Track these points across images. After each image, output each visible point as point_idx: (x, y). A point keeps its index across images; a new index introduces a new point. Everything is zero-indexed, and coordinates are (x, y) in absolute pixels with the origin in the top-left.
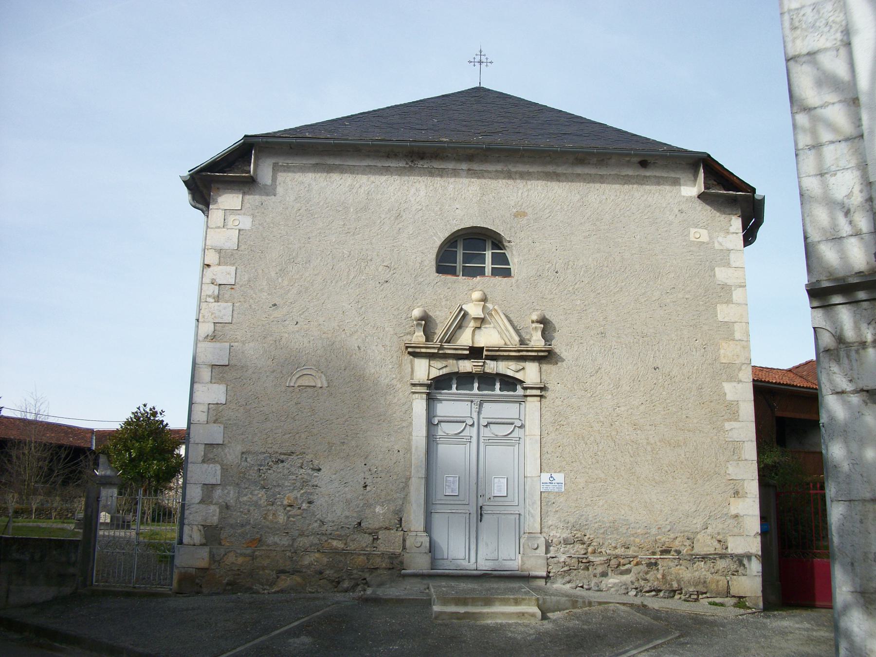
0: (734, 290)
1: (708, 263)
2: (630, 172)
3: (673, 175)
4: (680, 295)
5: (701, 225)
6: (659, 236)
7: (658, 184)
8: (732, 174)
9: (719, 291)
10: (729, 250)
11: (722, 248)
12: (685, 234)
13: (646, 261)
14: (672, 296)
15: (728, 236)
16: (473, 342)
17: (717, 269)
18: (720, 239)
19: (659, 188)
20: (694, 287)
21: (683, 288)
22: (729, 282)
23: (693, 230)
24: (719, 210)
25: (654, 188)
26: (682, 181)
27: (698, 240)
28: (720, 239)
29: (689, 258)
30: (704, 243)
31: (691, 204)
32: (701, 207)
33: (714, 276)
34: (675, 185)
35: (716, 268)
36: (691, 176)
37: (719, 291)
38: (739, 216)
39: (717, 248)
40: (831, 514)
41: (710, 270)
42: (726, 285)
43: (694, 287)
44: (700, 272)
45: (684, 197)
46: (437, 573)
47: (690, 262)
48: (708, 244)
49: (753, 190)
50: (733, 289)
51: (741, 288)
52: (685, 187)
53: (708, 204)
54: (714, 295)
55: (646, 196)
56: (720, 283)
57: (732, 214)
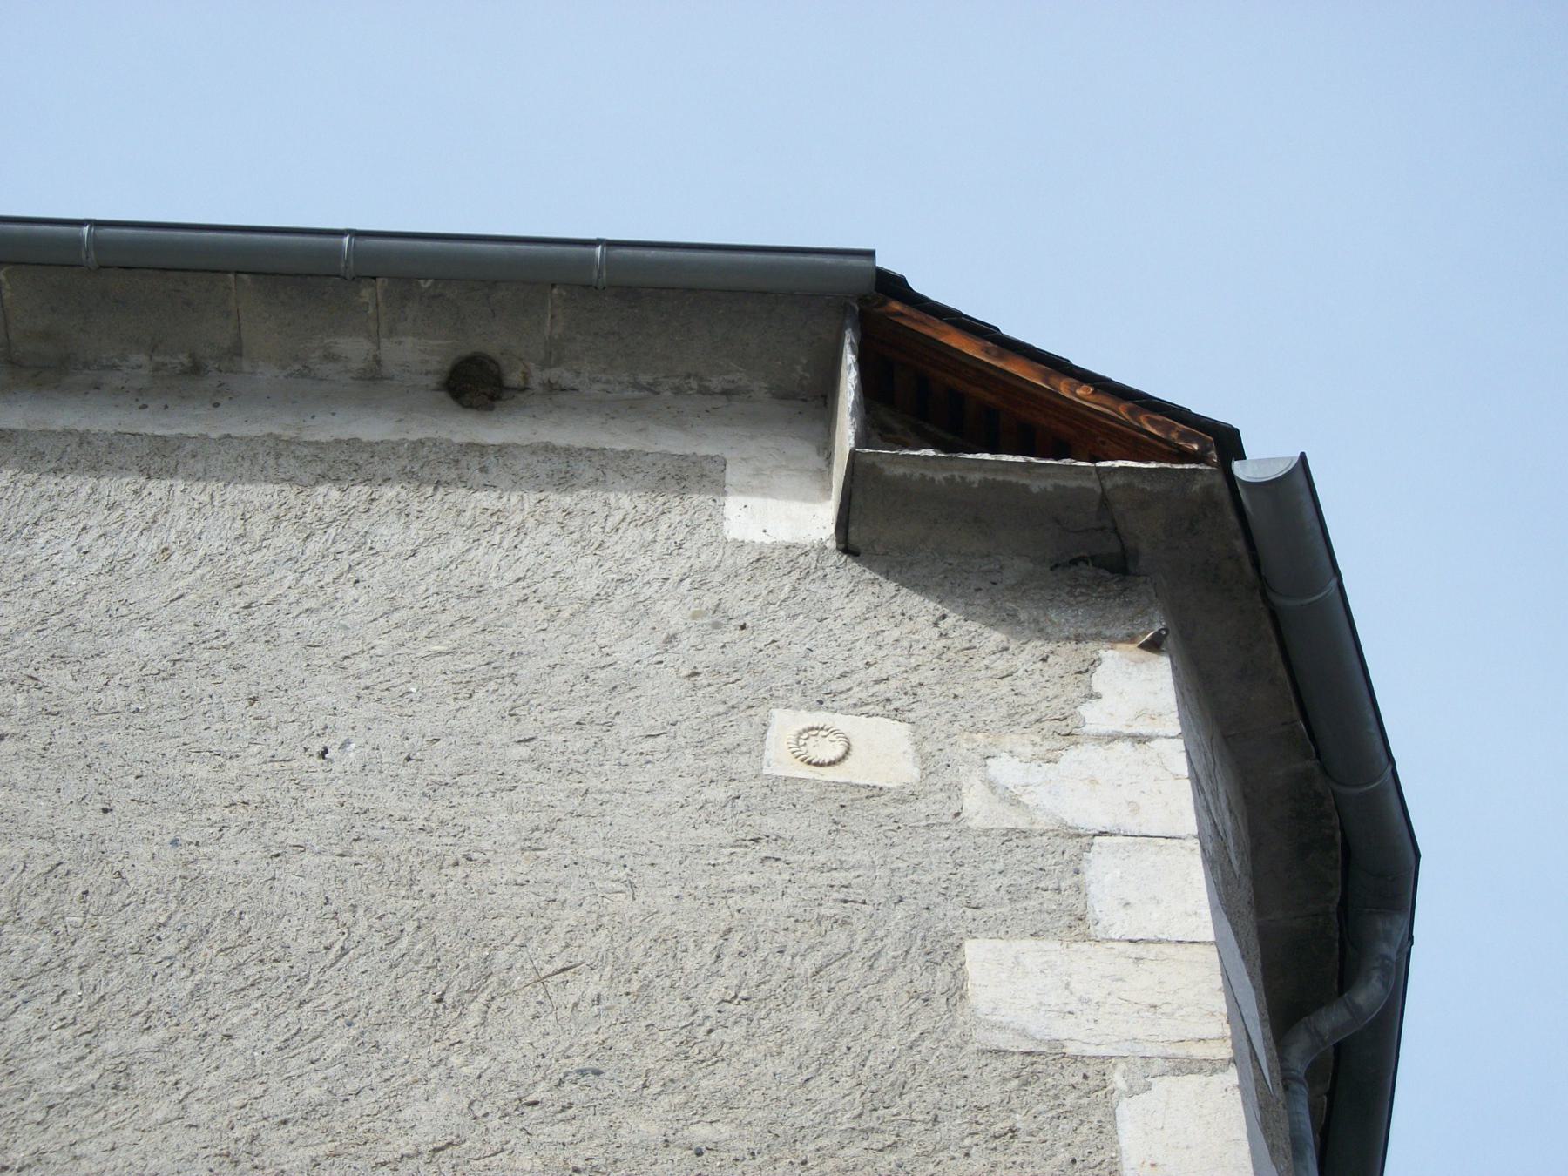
0: (1131, 1092)
1: (900, 912)
2: (374, 428)
3: (671, 442)
4: (645, 1126)
5: (858, 694)
6: (524, 751)
7: (565, 482)
8: (1060, 366)
9: (994, 1095)
10: (1082, 838)
11: (1022, 824)
12: (729, 740)
13: (377, 893)
14: (562, 1132)
15: (1072, 755)
16: (1209, 1067)
17: (976, 952)
18: (1006, 770)
19: (567, 501)
20: (779, 1065)
21: (676, 1069)
22: (1080, 1037)
23: (786, 723)
24: (1006, 619)
25: (520, 503)
26: (732, 475)
27: (829, 775)
28: (1006, 770)
29: (744, 879)
30: (875, 791)
31: (788, 582)
32: (860, 603)
33: (957, 993)
34: (683, 492)
35: (970, 947)
36: (804, 451)
37: (994, 1095)
38: (1154, 646)
39: (976, 822)
40: (1263, 1026)
41: (917, 961)
42: (1058, 1054)
43: (779, 1065)
44: (835, 971)
45: (741, 545)
46: (1269, 1060)
47: (750, 902)
48: (906, 796)
49: (1227, 442)
50: (1118, 1081)
51: (1194, 1080)
52: (755, 502)
53: (919, 586)
54: (953, 1127)
55: (458, 544)
56: (1000, 1040)
57: (1098, 637)
